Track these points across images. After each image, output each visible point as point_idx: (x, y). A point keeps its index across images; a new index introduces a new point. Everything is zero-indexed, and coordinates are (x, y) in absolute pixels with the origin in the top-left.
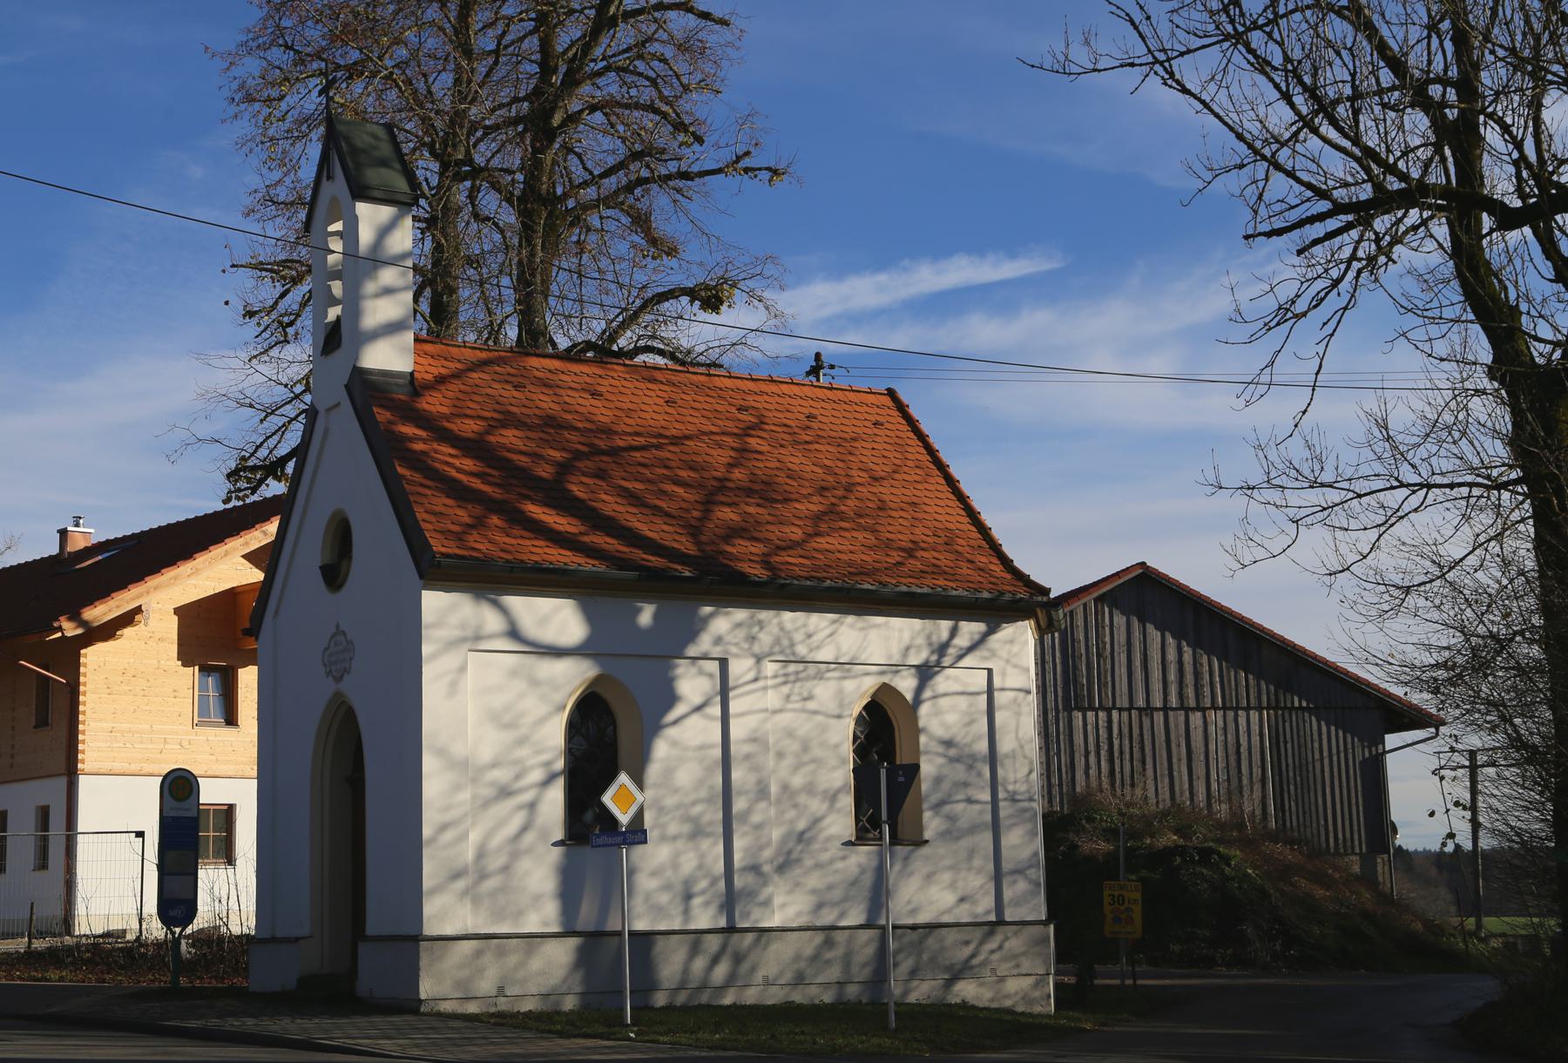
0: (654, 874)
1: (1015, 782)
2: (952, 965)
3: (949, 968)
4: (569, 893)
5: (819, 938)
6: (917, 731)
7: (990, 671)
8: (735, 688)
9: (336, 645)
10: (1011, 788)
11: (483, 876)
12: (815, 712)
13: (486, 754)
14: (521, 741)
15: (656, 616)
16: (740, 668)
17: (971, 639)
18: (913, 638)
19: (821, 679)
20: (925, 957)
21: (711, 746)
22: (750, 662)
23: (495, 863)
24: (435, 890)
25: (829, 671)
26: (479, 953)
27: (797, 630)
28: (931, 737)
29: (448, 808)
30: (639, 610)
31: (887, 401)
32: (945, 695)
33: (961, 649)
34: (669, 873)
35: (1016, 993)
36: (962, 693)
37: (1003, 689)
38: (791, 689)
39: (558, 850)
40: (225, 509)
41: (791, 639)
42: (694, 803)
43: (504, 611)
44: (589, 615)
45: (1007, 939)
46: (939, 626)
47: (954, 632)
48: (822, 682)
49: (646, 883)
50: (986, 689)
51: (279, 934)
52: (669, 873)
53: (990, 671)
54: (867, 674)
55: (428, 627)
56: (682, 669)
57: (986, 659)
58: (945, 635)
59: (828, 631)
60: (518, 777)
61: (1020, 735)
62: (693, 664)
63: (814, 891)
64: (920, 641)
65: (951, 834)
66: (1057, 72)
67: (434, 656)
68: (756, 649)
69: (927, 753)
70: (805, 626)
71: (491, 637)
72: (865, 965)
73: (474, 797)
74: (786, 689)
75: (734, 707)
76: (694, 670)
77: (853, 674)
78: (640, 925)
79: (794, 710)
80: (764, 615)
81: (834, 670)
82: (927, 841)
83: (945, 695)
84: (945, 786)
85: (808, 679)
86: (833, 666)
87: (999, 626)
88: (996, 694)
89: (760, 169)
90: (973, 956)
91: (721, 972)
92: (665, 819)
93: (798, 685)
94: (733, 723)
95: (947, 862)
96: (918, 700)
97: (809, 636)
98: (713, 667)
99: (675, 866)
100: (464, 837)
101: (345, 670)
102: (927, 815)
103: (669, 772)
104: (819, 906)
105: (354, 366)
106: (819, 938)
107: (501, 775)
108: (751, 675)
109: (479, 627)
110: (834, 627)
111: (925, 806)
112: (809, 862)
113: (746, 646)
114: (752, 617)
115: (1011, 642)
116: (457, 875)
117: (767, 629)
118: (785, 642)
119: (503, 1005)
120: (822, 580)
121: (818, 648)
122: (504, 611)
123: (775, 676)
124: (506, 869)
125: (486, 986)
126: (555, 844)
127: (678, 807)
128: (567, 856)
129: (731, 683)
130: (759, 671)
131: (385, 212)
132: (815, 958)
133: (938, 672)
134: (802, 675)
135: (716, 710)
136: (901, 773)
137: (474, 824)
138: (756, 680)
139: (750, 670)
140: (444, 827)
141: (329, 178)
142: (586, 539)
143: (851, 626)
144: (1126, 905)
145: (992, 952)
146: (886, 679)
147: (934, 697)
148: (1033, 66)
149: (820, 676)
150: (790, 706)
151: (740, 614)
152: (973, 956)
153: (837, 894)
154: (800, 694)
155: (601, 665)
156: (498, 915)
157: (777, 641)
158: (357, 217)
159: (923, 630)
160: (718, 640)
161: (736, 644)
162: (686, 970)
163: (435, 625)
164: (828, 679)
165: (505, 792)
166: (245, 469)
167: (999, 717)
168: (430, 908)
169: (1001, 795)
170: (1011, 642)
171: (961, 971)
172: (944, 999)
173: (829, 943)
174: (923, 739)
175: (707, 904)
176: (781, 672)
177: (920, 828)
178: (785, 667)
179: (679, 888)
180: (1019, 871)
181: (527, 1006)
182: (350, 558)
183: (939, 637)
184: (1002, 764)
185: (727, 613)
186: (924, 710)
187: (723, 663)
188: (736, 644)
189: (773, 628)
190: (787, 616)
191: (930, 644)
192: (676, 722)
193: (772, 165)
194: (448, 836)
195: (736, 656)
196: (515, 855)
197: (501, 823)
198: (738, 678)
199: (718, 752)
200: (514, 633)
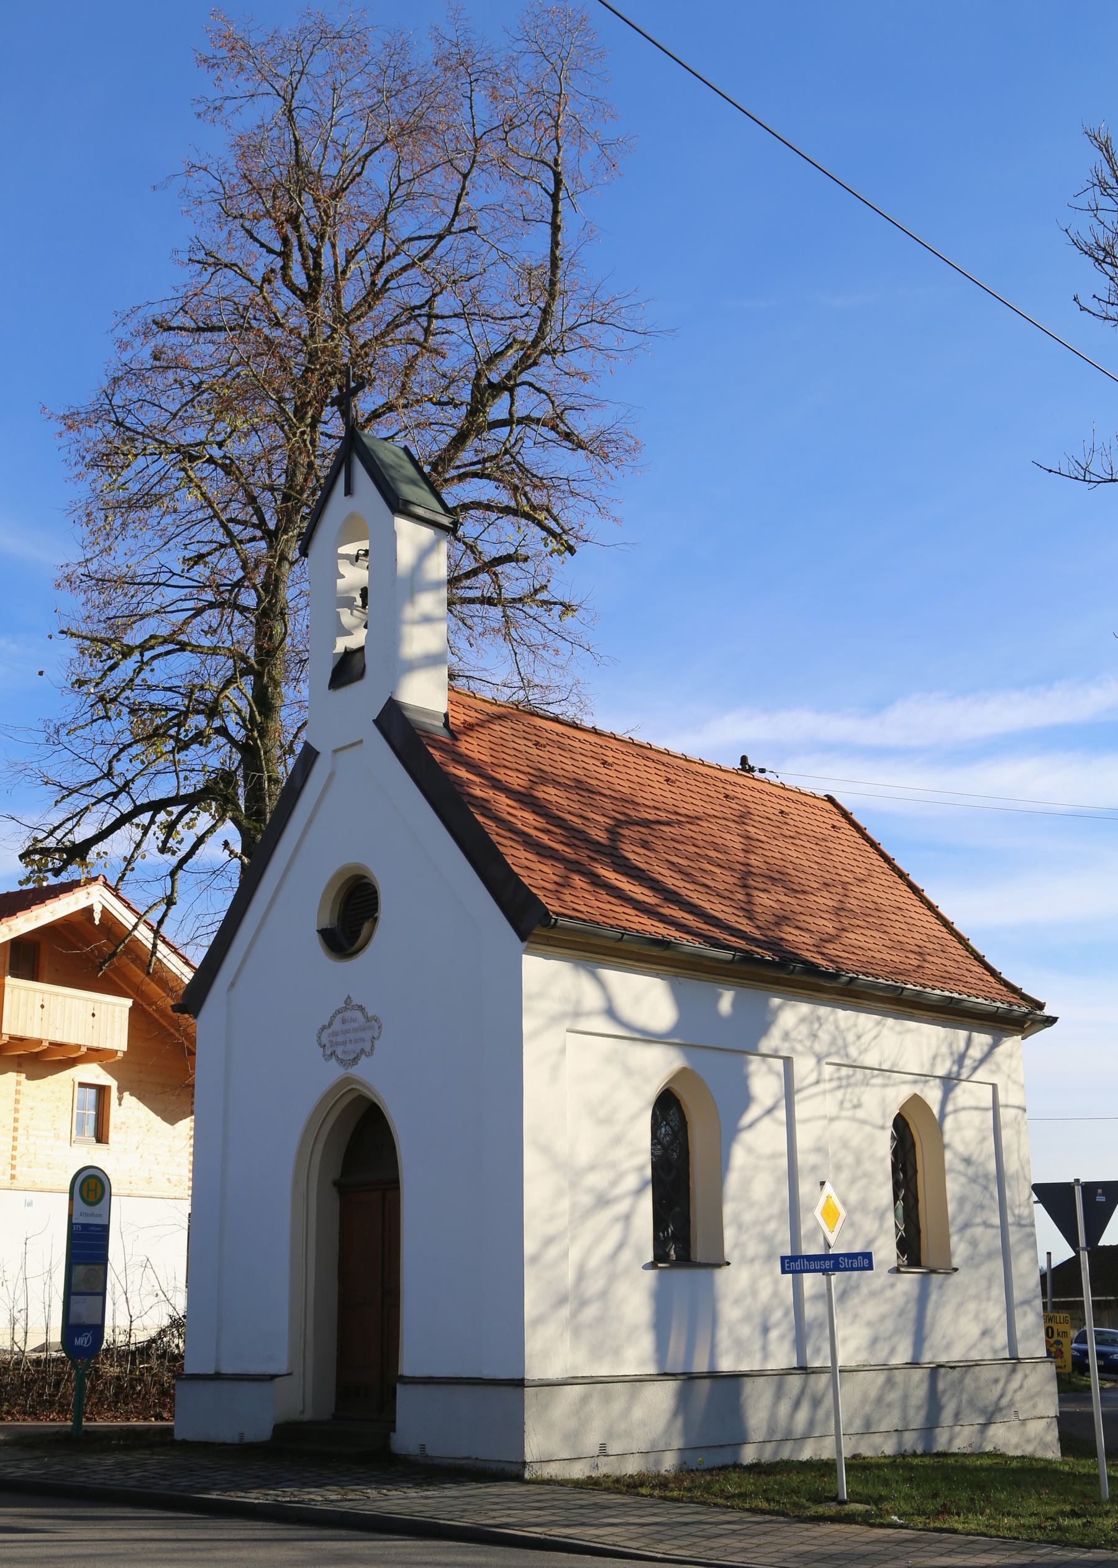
0: (737, 1302)
1: (1020, 1206)
2: (986, 1407)
3: (983, 1411)
4: (661, 1326)
5: (881, 1377)
6: (942, 1147)
7: (994, 1086)
8: (799, 1091)
9: (344, 1021)
10: (1017, 1212)
11: (583, 1303)
12: (864, 1122)
13: (584, 1155)
14: (617, 1140)
15: (735, 1004)
16: (804, 1067)
17: (982, 1050)
18: (938, 1047)
19: (867, 1084)
20: (965, 1397)
21: (780, 1155)
22: (812, 1061)
23: (594, 1286)
24: (539, 1320)
25: (873, 1077)
26: (585, 1399)
27: (849, 1029)
28: (955, 1153)
29: (552, 1218)
30: (719, 997)
31: (829, 806)
32: (963, 1109)
33: (975, 1061)
34: (748, 1301)
35: (1035, 1438)
36: (976, 1108)
37: (1007, 1106)
38: (844, 1095)
39: (651, 1274)
40: (21, 891)
41: (844, 1039)
42: (769, 1220)
43: (602, 984)
44: (680, 1001)
45: (1026, 1376)
46: (957, 1034)
47: (969, 1042)
48: (868, 1089)
49: (730, 1312)
50: (991, 1105)
51: (226, 1369)
52: (748, 1301)
53: (994, 1086)
54: (904, 1082)
55: (531, 997)
56: (755, 1065)
57: (992, 1072)
58: (962, 1045)
59: (872, 1034)
60: (614, 1183)
61: (1021, 1156)
62: (764, 1062)
63: (869, 1324)
64: (944, 1050)
65: (973, 1261)
66: (1076, 478)
67: (536, 1033)
68: (818, 1047)
69: (952, 1171)
70: (855, 1025)
71: (589, 1014)
72: (919, 1408)
73: (574, 1206)
74: (839, 1094)
75: (800, 1112)
76: (764, 1068)
77: (892, 1082)
78: (726, 1365)
79: (847, 1118)
80: (823, 1011)
81: (877, 1076)
82: (956, 1270)
83: (963, 1109)
84: (968, 1208)
85: (856, 1084)
86: (876, 1072)
87: (1001, 1040)
88: (1002, 1110)
89: (555, 603)
90: (1001, 1396)
91: (802, 1416)
92: (744, 1238)
93: (850, 1090)
94: (799, 1130)
95: (972, 1291)
96: (943, 1115)
97: (859, 1037)
98: (779, 1064)
99: (754, 1293)
100: (565, 1254)
101: (362, 1051)
102: (954, 1239)
103: (746, 1183)
104: (874, 1341)
105: (390, 698)
106: (881, 1377)
107: (597, 1180)
108: (813, 1078)
109: (578, 1002)
110: (880, 1027)
111: (952, 1230)
112: (864, 1290)
113: (808, 1043)
114: (812, 1012)
115: (1011, 1056)
116: (562, 1300)
117: (824, 1027)
118: (840, 1042)
119: (606, 1468)
120: (877, 976)
121: (866, 1050)
122: (602, 984)
123: (831, 1080)
124: (604, 1294)
125: (591, 1442)
126: (645, 1267)
127: (755, 1223)
128: (660, 1280)
129: (797, 1084)
130: (820, 1074)
131: (426, 533)
132: (879, 1400)
133: (956, 1085)
134: (852, 1080)
135: (781, 1114)
136: (1100, 1191)
137: (573, 1239)
138: (817, 1082)
139: (812, 1071)
140: (548, 1241)
141: (348, 491)
142: (661, 910)
143: (892, 1029)
144: (1056, 1338)
145: (1015, 1391)
146: (917, 1090)
147: (956, 1111)
148: (1050, 471)
149: (866, 1083)
150: (844, 1114)
151: (804, 1008)
152: (1001, 1396)
153: (889, 1325)
154: (851, 1101)
155: (688, 1056)
156: (596, 1352)
157: (833, 1042)
158: (395, 533)
159: (946, 1037)
160: (786, 1036)
161: (801, 1041)
162: (773, 1417)
163: (540, 995)
164: (874, 1086)
165: (603, 1201)
166: (36, 851)
167: (1006, 1135)
168: (535, 1342)
169: (1010, 1219)
170: (1011, 1056)
171: (993, 1414)
172: (980, 1447)
173: (890, 1383)
174: (948, 1156)
175: (782, 1337)
176: (836, 1075)
177: (947, 1253)
178: (838, 1070)
179: (757, 1320)
180: (1026, 1302)
181: (632, 1467)
182: (376, 919)
183: (958, 1046)
184: (1010, 1186)
185: (793, 1006)
186: (948, 1124)
187: (788, 1061)
188: (801, 1041)
189: (829, 1026)
190: (841, 1014)
191: (952, 1054)
192: (751, 1125)
193: (566, 601)
194: (553, 1252)
195: (801, 1054)
196: (612, 1279)
197: (599, 1239)
198: (804, 1079)
199: (784, 1162)
200: (611, 1013)
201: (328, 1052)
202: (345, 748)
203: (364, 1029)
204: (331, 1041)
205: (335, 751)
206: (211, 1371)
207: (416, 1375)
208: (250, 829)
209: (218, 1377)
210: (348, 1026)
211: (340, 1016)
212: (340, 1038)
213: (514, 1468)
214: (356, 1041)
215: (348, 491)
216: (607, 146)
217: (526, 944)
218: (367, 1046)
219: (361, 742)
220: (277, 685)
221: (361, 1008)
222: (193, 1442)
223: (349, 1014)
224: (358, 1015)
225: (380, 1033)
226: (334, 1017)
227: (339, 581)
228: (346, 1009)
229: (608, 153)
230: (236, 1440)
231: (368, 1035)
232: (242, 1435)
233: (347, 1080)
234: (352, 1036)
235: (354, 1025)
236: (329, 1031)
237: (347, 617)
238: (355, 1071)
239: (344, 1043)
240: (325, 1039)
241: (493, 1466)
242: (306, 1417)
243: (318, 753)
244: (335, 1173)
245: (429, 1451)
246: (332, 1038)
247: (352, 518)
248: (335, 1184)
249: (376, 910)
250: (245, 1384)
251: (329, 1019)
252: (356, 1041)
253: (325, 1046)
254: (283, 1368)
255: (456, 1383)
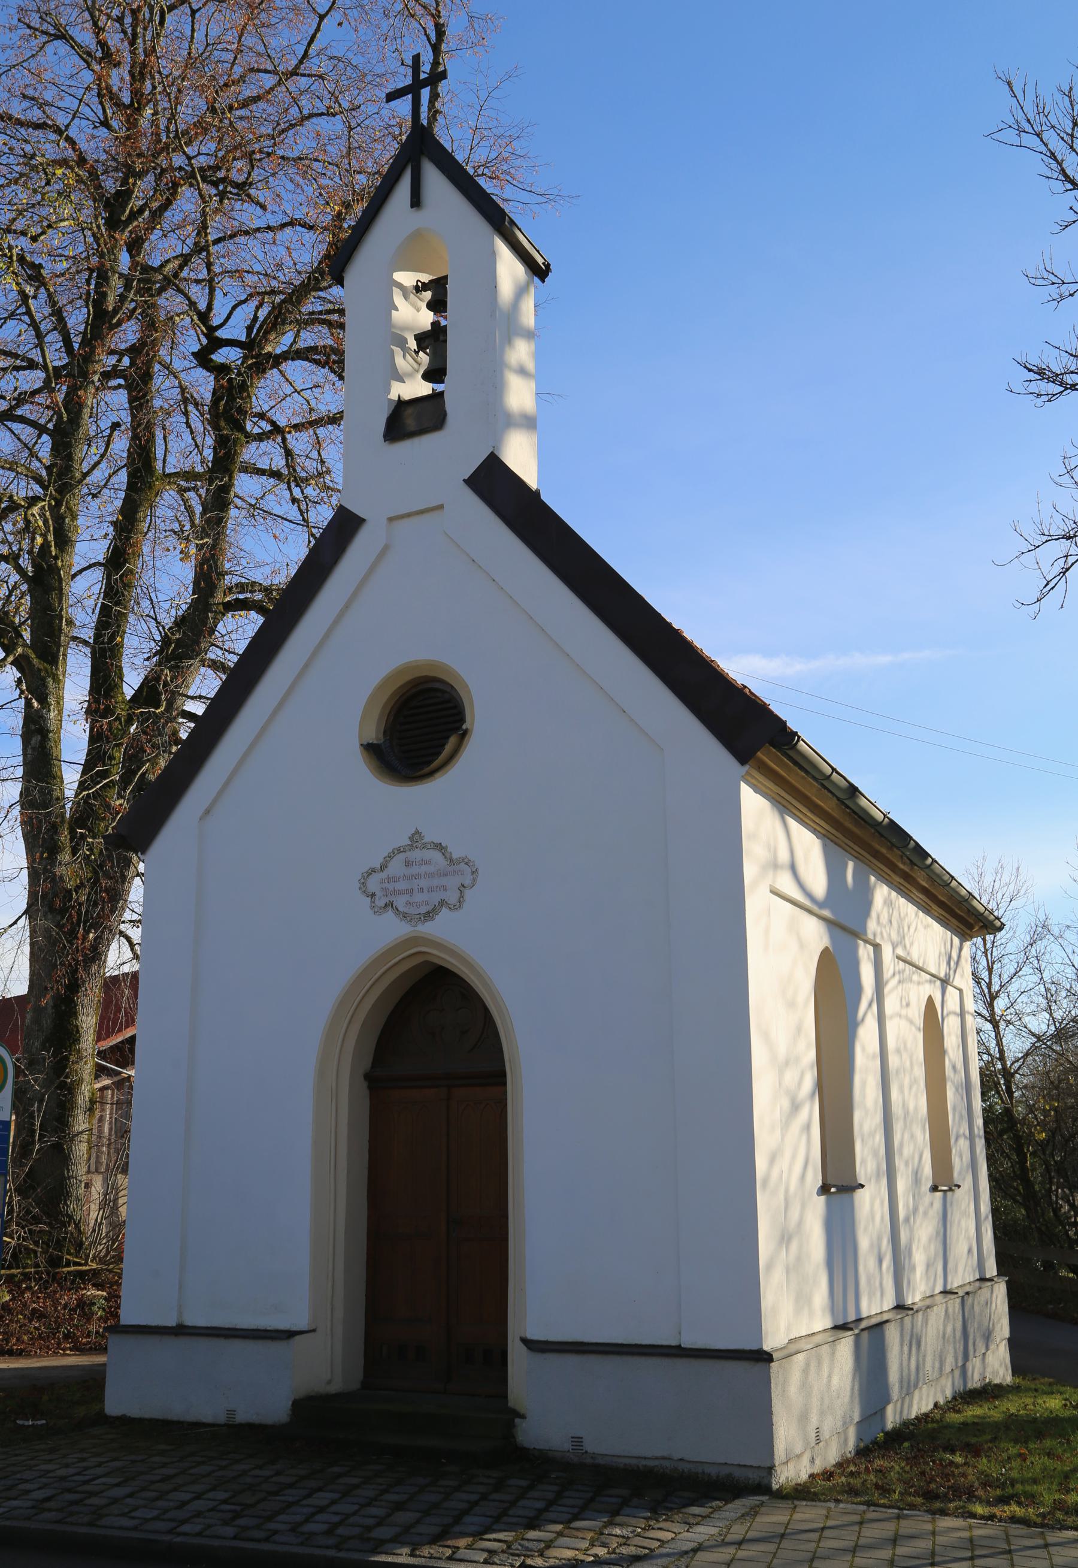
9: (408, 863)
101: (443, 903)
141: (416, 201)
155: (832, 937)
201: (381, 903)
202: (409, 515)
203: (446, 875)
204: (385, 889)
205: (391, 519)
206: (171, 1322)
207: (551, 1339)
208: (39, 670)
209: (181, 1331)
210: (414, 870)
211: (402, 856)
212: (402, 886)
213: (753, 1476)
214: (431, 890)
215: (416, 201)
216: (475, 19)
217: (747, 767)
218: (452, 897)
219: (441, 507)
220: (74, 517)
221: (439, 847)
222: (141, 1420)
223: (416, 855)
224: (436, 856)
225: (474, 880)
226: (390, 857)
227: (393, 312)
228: (411, 847)
229: (476, 25)
230: (222, 1419)
231: (453, 882)
232: (231, 1412)
233: (414, 940)
234: (424, 883)
235: (430, 869)
236: (383, 875)
237: (402, 363)
238: (428, 929)
239: (410, 892)
240: (373, 884)
241: (713, 1471)
242: (335, 1388)
243: (363, 520)
244: (367, 1063)
245: (590, 1446)
246: (386, 885)
247: (417, 236)
248: (367, 1077)
249: (462, 720)
250: (238, 1345)
251: (381, 860)
252: (431, 890)
253: (373, 895)
254: (302, 1324)
255: (632, 1354)
